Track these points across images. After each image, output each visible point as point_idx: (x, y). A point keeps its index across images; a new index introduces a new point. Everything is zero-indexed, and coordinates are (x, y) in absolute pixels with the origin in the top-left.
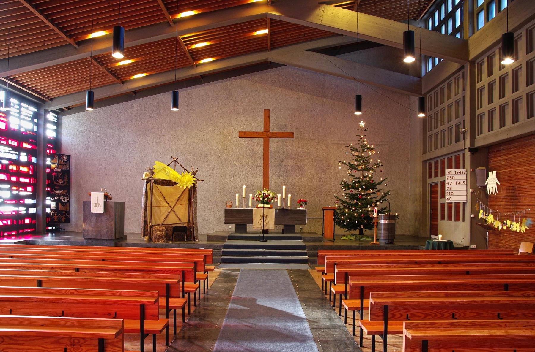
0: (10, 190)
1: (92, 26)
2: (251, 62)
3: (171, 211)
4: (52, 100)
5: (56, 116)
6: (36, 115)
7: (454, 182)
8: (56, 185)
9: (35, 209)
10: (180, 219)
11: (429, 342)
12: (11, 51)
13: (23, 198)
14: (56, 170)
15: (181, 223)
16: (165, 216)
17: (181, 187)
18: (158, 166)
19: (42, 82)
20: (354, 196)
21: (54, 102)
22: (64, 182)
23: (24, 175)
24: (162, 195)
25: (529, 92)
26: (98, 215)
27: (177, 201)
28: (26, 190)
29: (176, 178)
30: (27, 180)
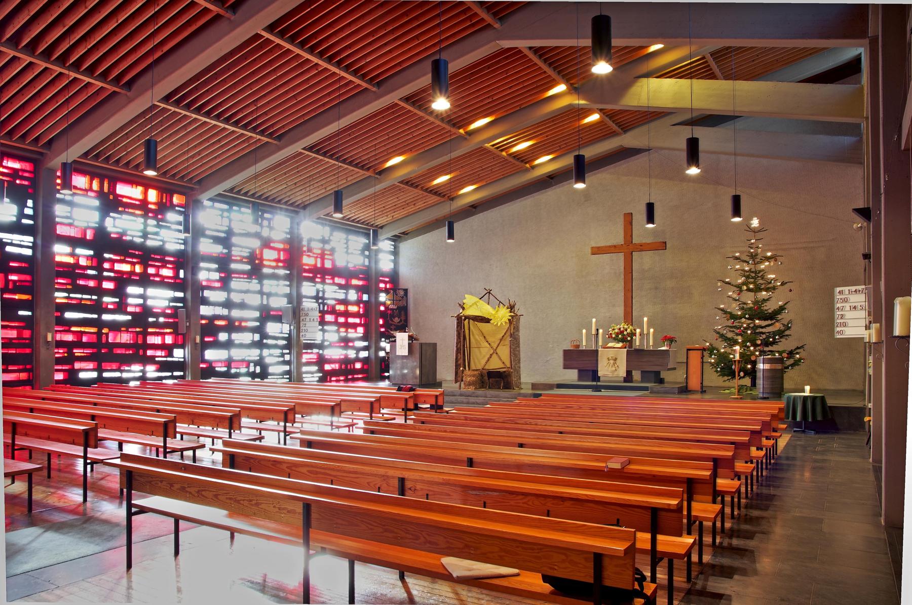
0: (338, 331)
1: (388, 154)
2: (609, 150)
3: (493, 354)
4: (382, 227)
5: (393, 243)
6: (367, 247)
7: (847, 306)
8: (392, 325)
9: (367, 352)
10: (503, 363)
11: (4, 380)
12: (340, 183)
13: (352, 340)
14: (392, 307)
15: (505, 368)
16: (486, 359)
17: (499, 324)
18: (469, 300)
19: (363, 212)
20: (756, 329)
21: (385, 229)
22: (401, 321)
23: (354, 315)
24: (483, 334)
25: (633, 227)
26: (403, 357)
27: (501, 340)
28: (356, 332)
29: (489, 314)
30: (357, 321)
